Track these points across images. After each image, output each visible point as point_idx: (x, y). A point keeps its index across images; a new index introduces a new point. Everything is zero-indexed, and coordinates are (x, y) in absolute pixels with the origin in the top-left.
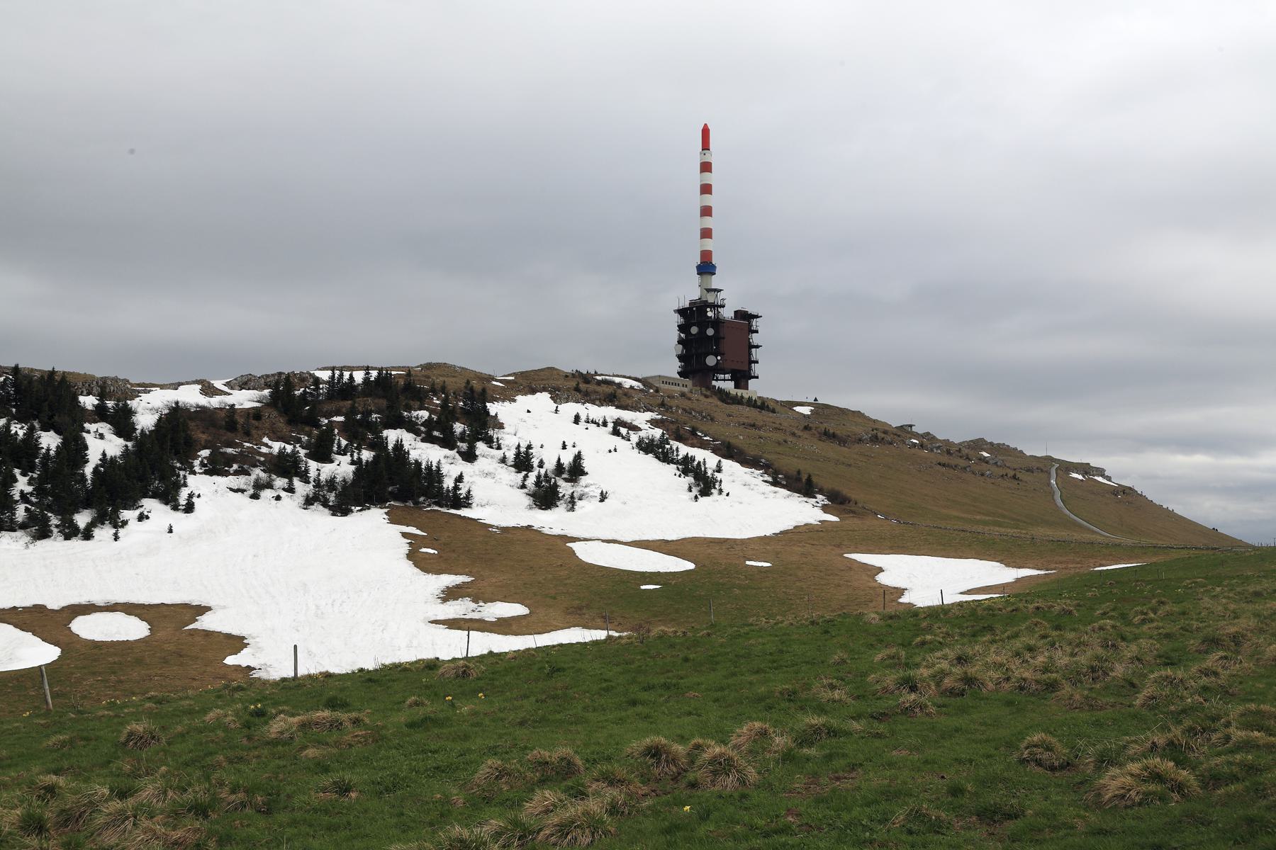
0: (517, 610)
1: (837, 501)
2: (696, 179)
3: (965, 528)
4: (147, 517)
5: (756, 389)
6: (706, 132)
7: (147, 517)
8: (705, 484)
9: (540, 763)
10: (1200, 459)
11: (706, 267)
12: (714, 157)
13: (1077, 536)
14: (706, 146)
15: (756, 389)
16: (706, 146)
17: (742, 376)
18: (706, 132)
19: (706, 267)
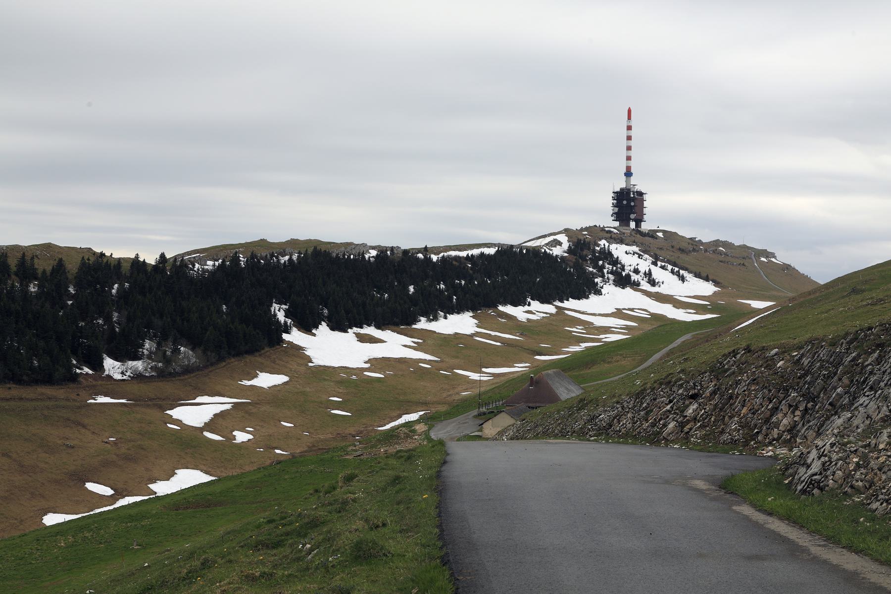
0: (566, 312)
1: (716, 283)
2: (625, 133)
3: (678, 254)
4: (683, 281)
5: (645, 227)
6: (629, 111)
7: (683, 281)
8: (683, 279)
9: (395, 480)
10: (493, 333)
11: (628, 174)
12: (633, 123)
13: (780, 294)
14: (629, 118)
15: (645, 227)
16: (629, 118)
17: (639, 221)
18: (629, 111)
19: (628, 174)
